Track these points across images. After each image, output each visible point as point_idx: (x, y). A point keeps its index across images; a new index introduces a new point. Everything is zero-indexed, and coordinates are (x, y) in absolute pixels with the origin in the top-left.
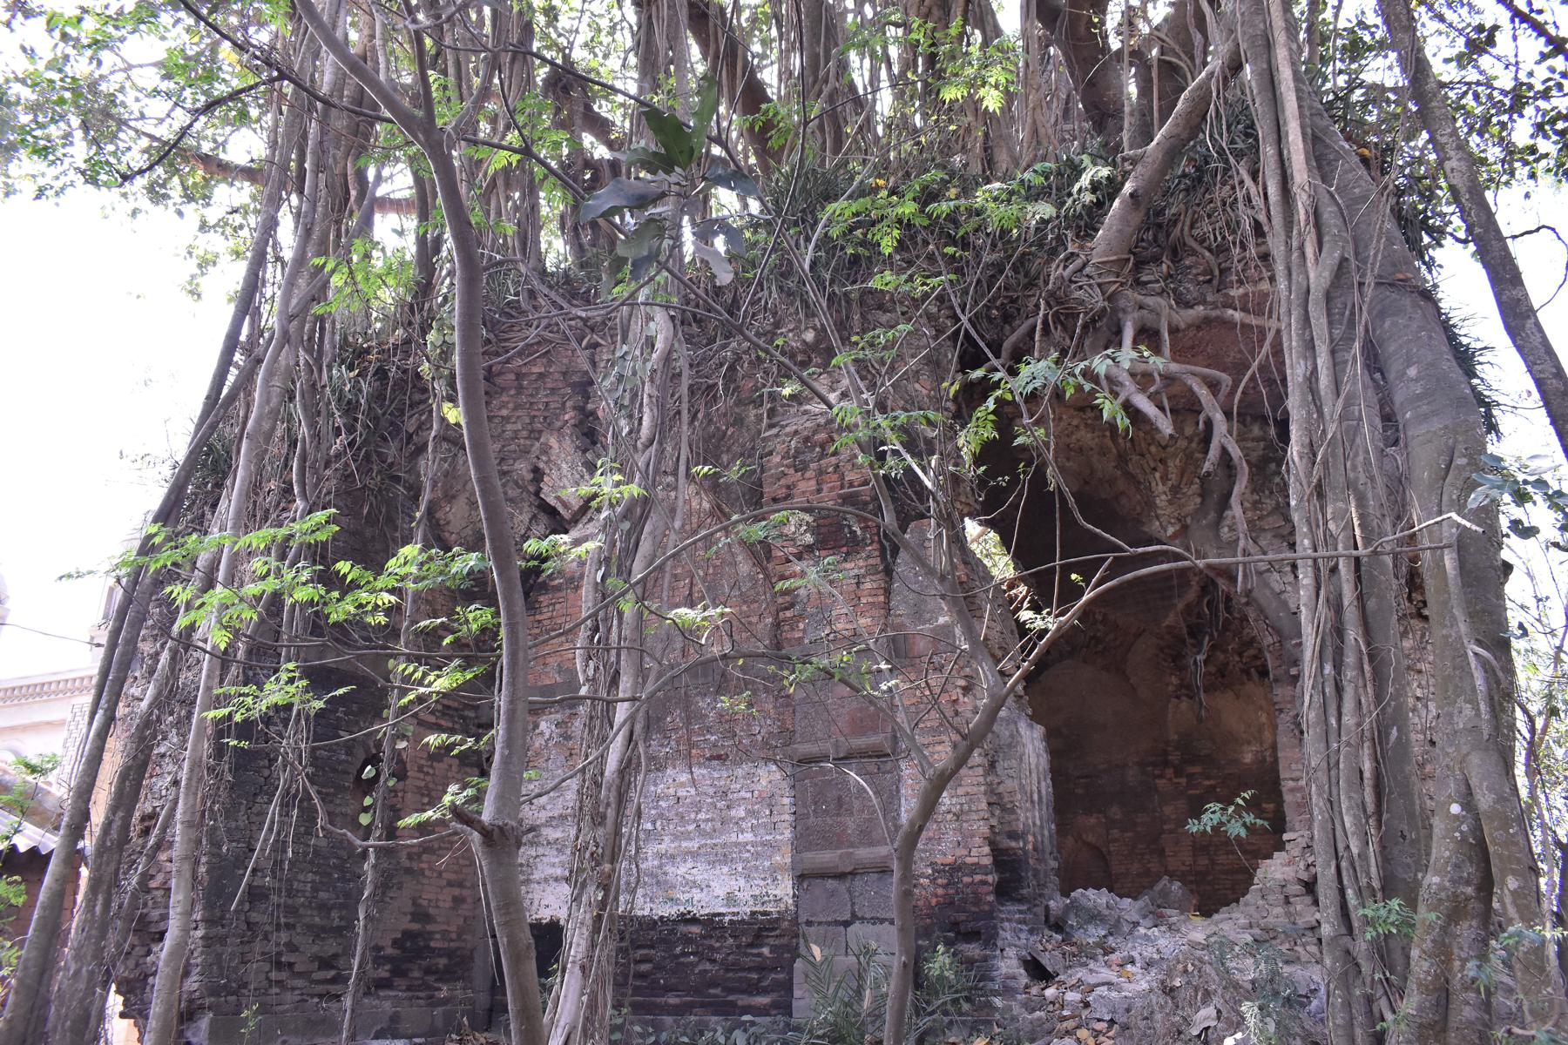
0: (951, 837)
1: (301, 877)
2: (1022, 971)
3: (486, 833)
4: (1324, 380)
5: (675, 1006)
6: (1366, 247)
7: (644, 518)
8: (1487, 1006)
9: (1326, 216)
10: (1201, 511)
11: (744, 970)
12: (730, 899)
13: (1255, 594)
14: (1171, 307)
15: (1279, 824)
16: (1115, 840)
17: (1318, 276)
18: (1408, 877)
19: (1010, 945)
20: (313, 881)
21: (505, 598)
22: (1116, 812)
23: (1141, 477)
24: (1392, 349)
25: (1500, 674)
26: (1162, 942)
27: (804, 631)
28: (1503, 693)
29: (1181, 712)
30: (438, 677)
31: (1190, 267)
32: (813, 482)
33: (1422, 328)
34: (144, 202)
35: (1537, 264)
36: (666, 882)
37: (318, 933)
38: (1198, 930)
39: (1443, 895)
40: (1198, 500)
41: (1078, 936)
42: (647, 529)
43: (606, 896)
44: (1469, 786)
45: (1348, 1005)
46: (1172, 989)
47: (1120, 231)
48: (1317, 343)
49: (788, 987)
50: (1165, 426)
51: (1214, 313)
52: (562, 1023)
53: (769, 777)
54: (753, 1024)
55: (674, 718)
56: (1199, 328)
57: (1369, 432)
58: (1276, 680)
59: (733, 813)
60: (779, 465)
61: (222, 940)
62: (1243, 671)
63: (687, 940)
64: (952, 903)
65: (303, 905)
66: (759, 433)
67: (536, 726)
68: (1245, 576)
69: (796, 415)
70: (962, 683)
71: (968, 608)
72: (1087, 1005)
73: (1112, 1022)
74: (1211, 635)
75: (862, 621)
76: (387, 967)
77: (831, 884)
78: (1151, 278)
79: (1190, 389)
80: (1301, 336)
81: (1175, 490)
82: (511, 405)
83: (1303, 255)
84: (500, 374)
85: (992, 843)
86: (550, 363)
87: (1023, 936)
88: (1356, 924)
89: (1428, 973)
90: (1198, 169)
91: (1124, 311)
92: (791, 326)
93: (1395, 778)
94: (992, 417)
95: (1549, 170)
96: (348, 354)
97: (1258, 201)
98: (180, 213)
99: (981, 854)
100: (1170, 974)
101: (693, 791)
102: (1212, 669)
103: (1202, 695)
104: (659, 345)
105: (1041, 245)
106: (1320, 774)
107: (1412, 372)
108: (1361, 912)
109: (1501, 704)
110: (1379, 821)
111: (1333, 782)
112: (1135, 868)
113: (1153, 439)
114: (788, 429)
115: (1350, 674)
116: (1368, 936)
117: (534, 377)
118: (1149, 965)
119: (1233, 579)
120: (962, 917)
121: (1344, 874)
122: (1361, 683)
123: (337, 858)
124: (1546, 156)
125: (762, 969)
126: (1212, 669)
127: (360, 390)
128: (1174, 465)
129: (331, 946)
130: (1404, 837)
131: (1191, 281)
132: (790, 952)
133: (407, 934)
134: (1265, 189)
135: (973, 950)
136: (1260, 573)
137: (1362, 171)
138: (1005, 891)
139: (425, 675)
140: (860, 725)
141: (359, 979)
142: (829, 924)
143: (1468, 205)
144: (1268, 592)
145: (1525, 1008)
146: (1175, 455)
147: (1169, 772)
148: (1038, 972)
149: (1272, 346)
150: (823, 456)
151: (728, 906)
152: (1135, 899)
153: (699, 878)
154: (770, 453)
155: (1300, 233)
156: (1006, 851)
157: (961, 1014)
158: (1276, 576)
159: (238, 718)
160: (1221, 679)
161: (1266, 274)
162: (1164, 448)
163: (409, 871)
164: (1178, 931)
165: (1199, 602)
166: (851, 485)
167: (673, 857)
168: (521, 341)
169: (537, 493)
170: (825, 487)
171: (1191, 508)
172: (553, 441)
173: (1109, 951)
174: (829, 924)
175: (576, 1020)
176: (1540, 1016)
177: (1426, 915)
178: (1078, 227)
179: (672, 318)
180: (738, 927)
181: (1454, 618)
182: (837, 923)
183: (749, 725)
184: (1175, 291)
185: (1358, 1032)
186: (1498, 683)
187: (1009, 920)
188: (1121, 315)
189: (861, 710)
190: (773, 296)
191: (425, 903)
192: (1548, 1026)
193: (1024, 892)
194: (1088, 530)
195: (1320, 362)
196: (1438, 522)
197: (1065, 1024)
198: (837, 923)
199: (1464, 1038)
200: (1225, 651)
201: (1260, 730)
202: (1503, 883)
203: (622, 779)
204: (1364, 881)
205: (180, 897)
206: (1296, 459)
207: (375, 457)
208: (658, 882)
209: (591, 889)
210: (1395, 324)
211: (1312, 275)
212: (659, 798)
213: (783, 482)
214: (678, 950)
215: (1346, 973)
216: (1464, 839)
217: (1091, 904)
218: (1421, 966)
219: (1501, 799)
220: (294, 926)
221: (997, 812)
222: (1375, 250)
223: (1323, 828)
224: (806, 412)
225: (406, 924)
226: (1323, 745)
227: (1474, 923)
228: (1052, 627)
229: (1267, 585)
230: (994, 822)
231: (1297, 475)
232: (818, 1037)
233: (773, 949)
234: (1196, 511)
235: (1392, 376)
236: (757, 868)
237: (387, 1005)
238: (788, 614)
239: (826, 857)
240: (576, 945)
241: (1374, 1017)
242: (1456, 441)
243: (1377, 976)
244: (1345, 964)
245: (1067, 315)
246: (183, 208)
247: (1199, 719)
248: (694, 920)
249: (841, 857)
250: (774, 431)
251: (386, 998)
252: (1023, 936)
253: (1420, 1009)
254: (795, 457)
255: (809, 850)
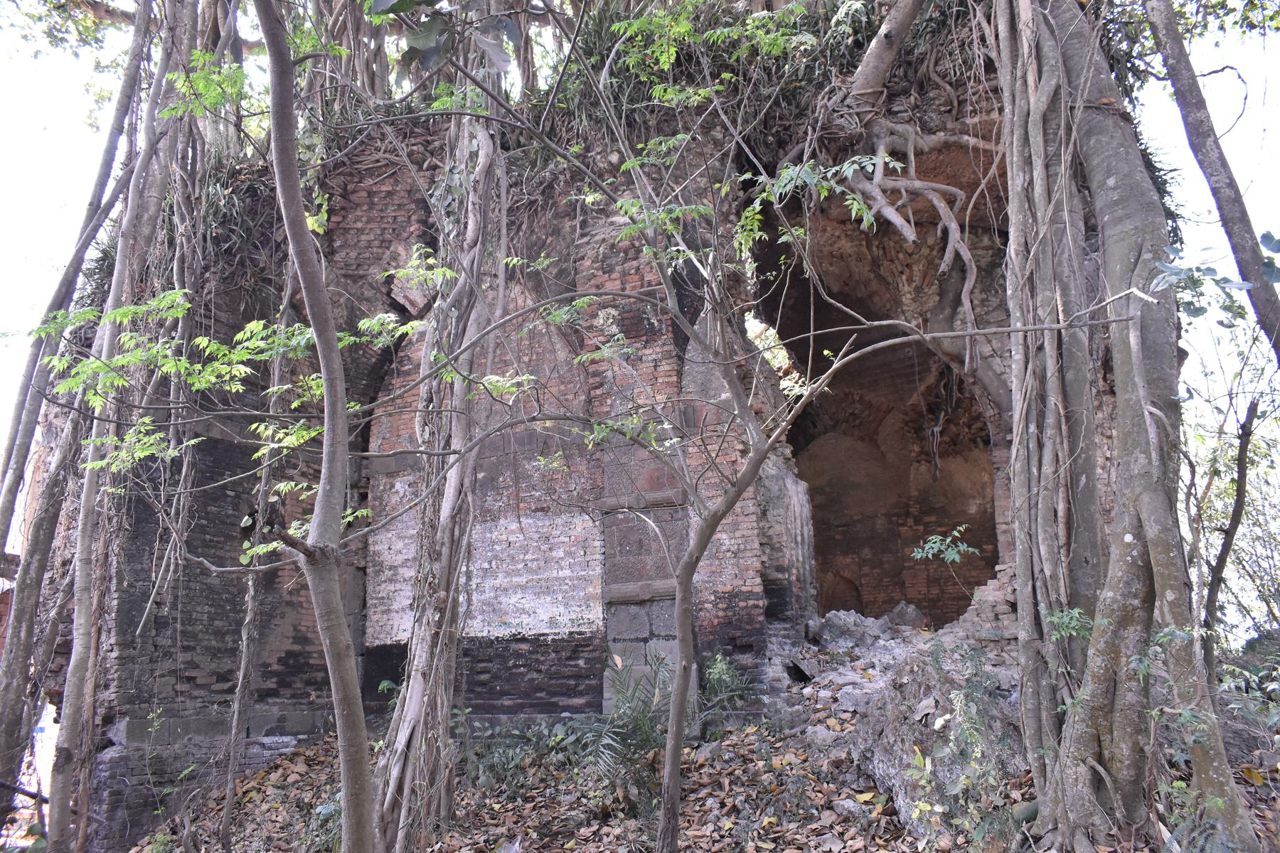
0: (730, 571)
1: (199, 609)
2: (786, 675)
3: (309, 554)
4: (1039, 189)
5: (508, 707)
6: (1078, 76)
7: (470, 307)
8: (1145, 691)
9: (1045, 49)
10: (939, 307)
11: (564, 677)
12: (552, 622)
13: (980, 373)
14: (917, 133)
15: (994, 559)
16: (867, 575)
17: (1037, 101)
18: (1089, 593)
19: (776, 655)
20: (209, 612)
21: (325, 357)
22: (866, 552)
23: (890, 279)
24: (1095, 163)
25: (1169, 429)
26: (897, 651)
27: (611, 406)
28: (1171, 448)
29: (920, 474)
30: (287, 434)
31: (934, 99)
32: (618, 282)
33: (1121, 145)
34: (44, 42)
35: (1219, 99)
36: (500, 610)
37: (215, 654)
38: (923, 641)
39: (1115, 606)
40: (937, 298)
41: (831, 647)
42: (473, 316)
43: (442, 617)
44: (1140, 519)
45: (1037, 693)
46: (901, 686)
47: (876, 67)
48: (1034, 158)
49: (599, 690)
50: (910, 233)
51: (953, 139)
52: (408, 719)
53: (583, 525)
54: (571, 719)
55: (506, 478)
56: (940, 151)
57: (1072, 236)
58: (995, 445)
59: (554, 554)
60: (591, 267)
61: (133, 660)
62: (971, 440)
63: (518, 655)
64: (730, 623)
65: (201, 631)
66: (573, 241)
67: (393, 486)
68: (971, 358)
69: (603, 226)
70: (741, 447)
71: (742, 379)
72: (836, 700)
73: (855, 712)
74: (946, 411)
75: (658, 397)
76: (274, 680)
77: (633, 609)
78: (901, 108)
79: (933, 207)
80: (1021, 153)
81: (918, 290)
82: (364, 219)
83: (1025, 83)
84: (354, 192)
85: (763, 576)
86: (397, 182)
87: (787, 648)
88: (1045, 630)
89: (1100, 667)
90: (943, 13)
91: (878, 136)
92: (599, 150)
93: (1082, 515)
94: (758, 217)
95: (1236, 23)
96: (224, 175)
97: (990, 40)
98: (76, 55)
99: (754, 584)
100: (899, 674)
101: (521, 537)
102: (946, 439)
103: (938, 460)
104: (481, 160)
105: (810, 81)
106: (1022, 513)
107: (1111, 182)
108: (1049, 619)
109: (1169, 454)
110: (1068, 551)
111: (1033, 519)
112: (882, 596)
113: (901, 247)
114: (597, 238)
115: (1049, 432)
116: (1054, 638)
117: (383, 195)
118: (886, 668)
119: (962, 362)
120: (739, 633)
121: (1038, 591)
122: (1058, 440)
123: (229, 593)
124: (1234, 10)
125: (577, 677)
126: (946, 439)
127: (234, 205)
128: (918, 269)
129: (226, 664)
130: (1087, 562)
131: (934, 111)
132: (601, 662)
133: (290, 654)
134: (996, 27)
135: (746, 659)
136: (984, 358)
137: (1081, 14)
138: (774, 612)
139: (275, 432)
140: (656, 484)
141: (245, 686)
142: (631, 640)
143: (1164, 39)
144: (990, 373)
145: (1175, 692)
146: (918, 261)
147: (910, 521)
148: (798, 675)
149: (998, 167)
150: (626, 260)
151: (550, 627)
152: (876, 618)
153: (527, 606)
154: (582, 258)
155: (1023, 65)
156: (774, 582)
157: (735, 709)
158: (998, 360)
159: (114, 469)
160: (953, 447)
161: (996, 105)
162: (910, 255)
163: (289, 603)
164: (910, 642)
165: (937, 385)
166: (650, 284)
167: (506, 590)
168: (373, 170)
169: (389, 294)
170: (628, 286)
171: (930, 304)
172: (401, 250)
173: (854, 659)
174: (631, 640)
175: (419, 716)
176: (1186, 698)
177: (1101, 621)
178: (842, 65)
179: (492, 136)
180: (558, 645)
181: (1134, 384)
182: (638, 640)
183: (567, 483)
184: (920, 119)
185: (1044, 714)
186: (1167, 436)
187: (776, 636)
188: (875, 140)
189: (657, 470)
190: (582, 123)
191: (304, 629)
192: (1192, 706)
193: (789, 613)
194: (830, 304)
195: (1035, 174)
196: (1126, 298)
197: (818, 715)
198: (638, 640)
199: (1126, 717)
200: (957, 425)
201: (983, 486)
202: (1163, 596)
203: (455, 523)
204: (1053, 597)
205: (82, 621)
206: (1013, 256)
207: (248, 262)
208: (494, 610)
209: (429, 612)
210: (1099, 141)
211: (1032, 100)
212: (494, 543)
213: (593, 282)
214: (511, 663)
215: (1037, 669)
216: (1134, 562)
217: (841, 623)
218: (1096, 662)
219: (1165, 530)
220: (194, 648)
221: (768, 551)
222: (1085, 79)
223: (1024, 556)
224: (612, 223)
225: (288, 645)
226: (1026, 489)
227: (1139, 628)
228: (806, 394)
229: (990, 367)
230: (765, 558)
231: (1013, 269)
232: (619, 727)
233: (588, 661)
234: (935, 307)
235: (1094, 186)
236: (574, 598)
237: (275, 709)
238: (598, 392)
239: (630, 588)
240: (419, 657)
241: (1055, 701)
242: (1144, 240)
243: (1060, 670)
244: (1036, 661)
245: (829, 139)
246: (80, 51)
247: (935, 479)
248: (524, 640)
249: (641, 587)
250: (586, 239)
251: (274, 704)
252: (787, 648)
253: (1093, 695)
254: (603, 261)
255: (616, 582)
